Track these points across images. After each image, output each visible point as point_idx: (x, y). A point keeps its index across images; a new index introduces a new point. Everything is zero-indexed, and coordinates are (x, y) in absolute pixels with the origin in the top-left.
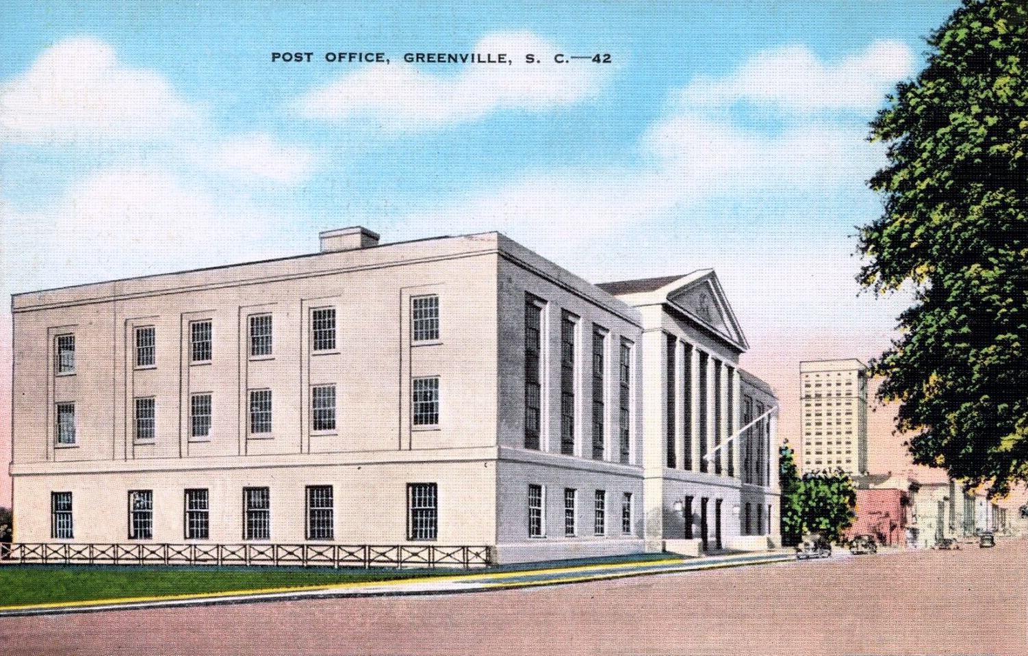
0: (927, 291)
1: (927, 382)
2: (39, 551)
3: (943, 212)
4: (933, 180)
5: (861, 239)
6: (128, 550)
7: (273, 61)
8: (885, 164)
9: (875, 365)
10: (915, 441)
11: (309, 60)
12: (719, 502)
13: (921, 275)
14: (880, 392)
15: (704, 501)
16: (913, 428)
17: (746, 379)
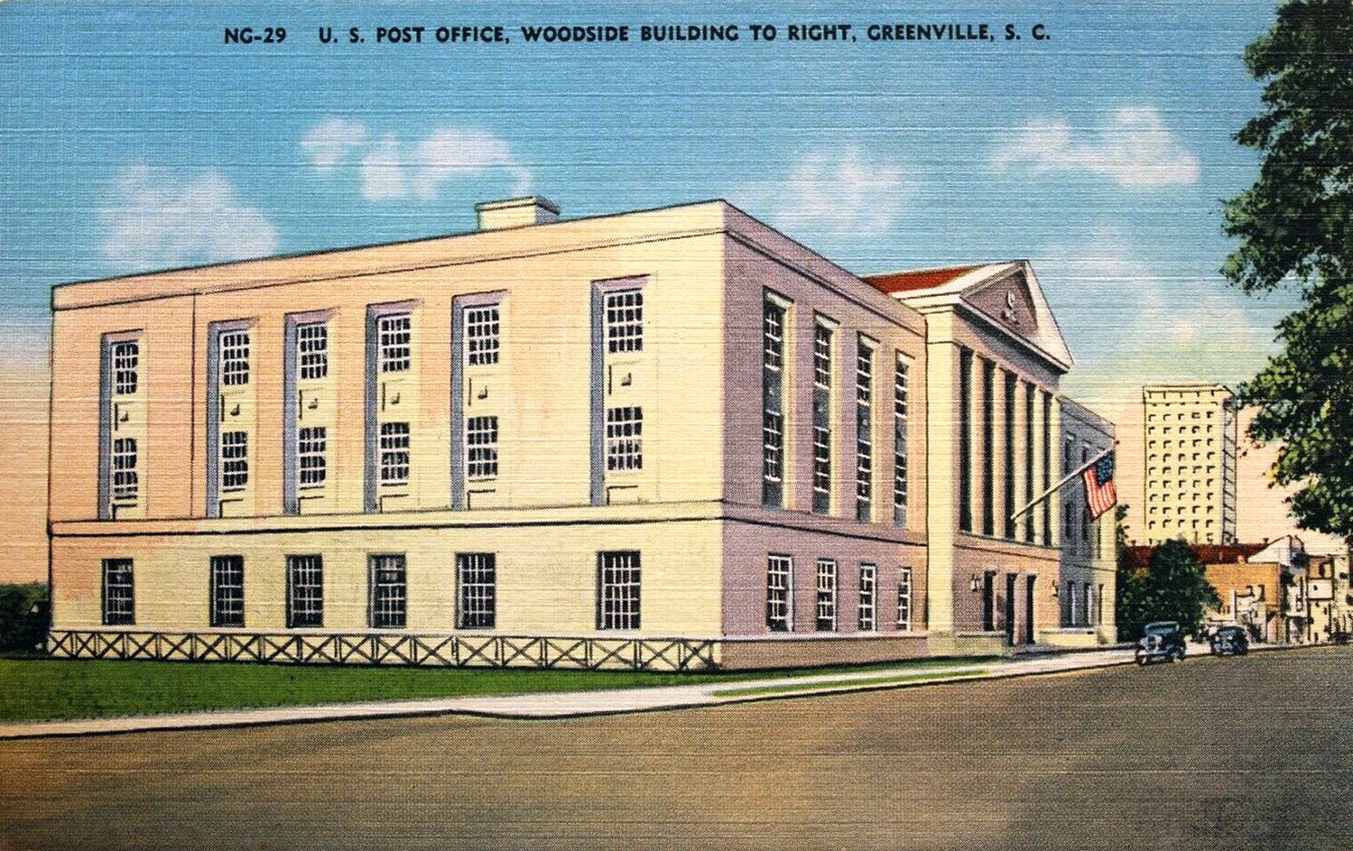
0: (1316, 288)
1: (1318, 414)
2: (254, 648)
3: (1339, 178)
4: (1325, 133)
5: (1227, 216)
6: (521, 657)
7: (379, 40)
8: (1261, 110)
9: (1246, 390)
10: (1300, 496)
11: (419, 40)
12: (1031, 579)
13: (1309, 267)
14: (1252, 428)
15: (1011, 578)
16: (1298, 479)
17: (1067, 408)
